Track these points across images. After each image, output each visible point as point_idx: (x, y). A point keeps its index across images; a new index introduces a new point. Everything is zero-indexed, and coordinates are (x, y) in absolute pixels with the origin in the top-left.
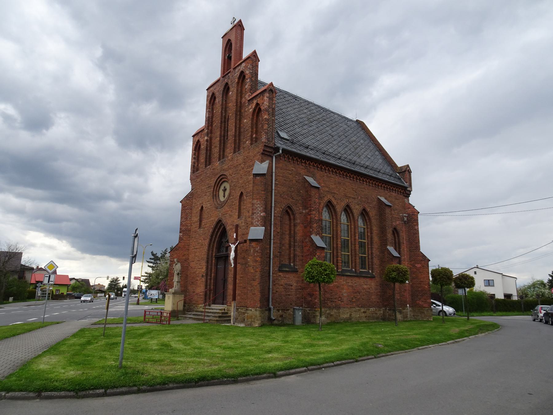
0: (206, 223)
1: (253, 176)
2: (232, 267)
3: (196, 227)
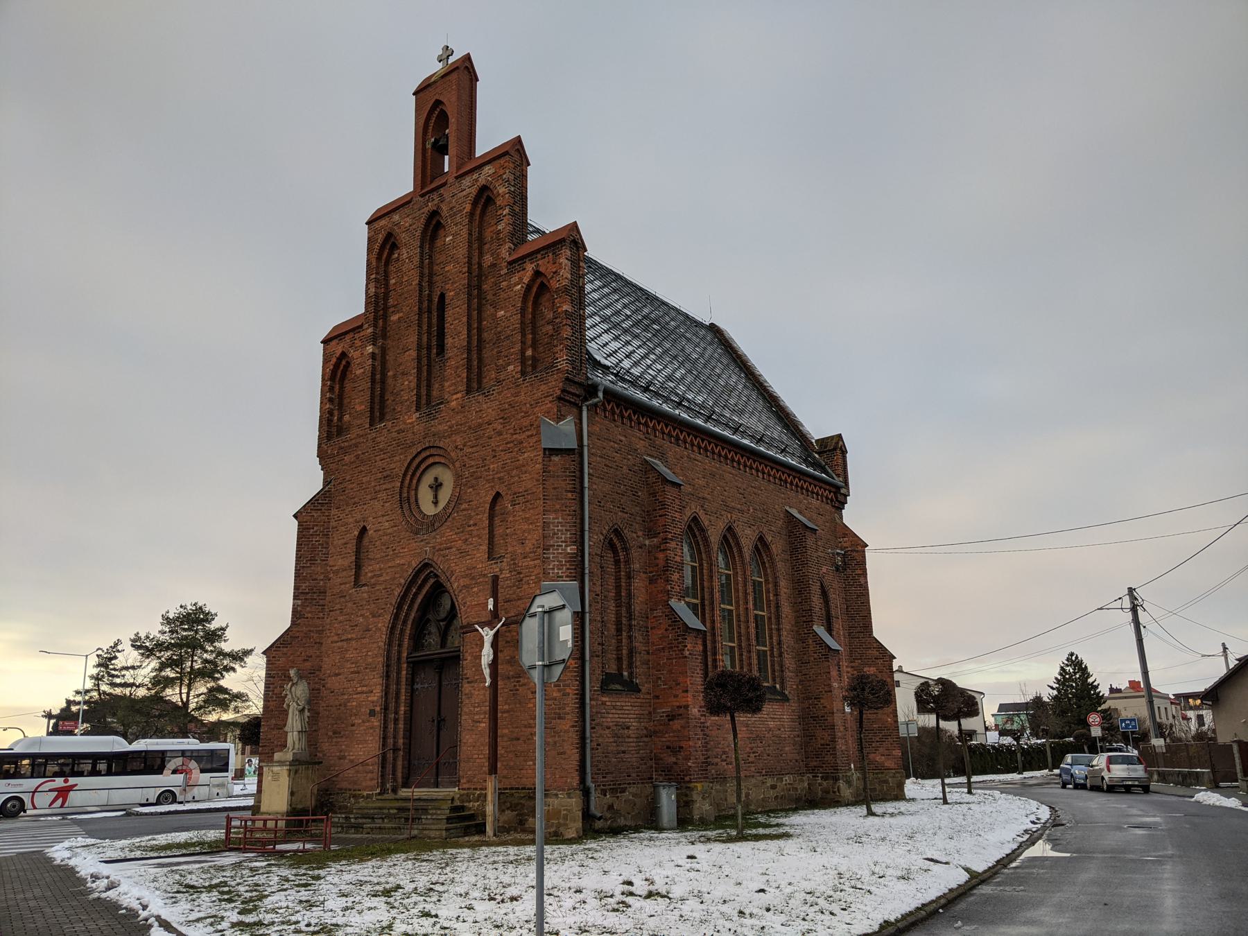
0: (379, 573)
1: (544, 454)
2: (487, 684)
3: (345, 583)
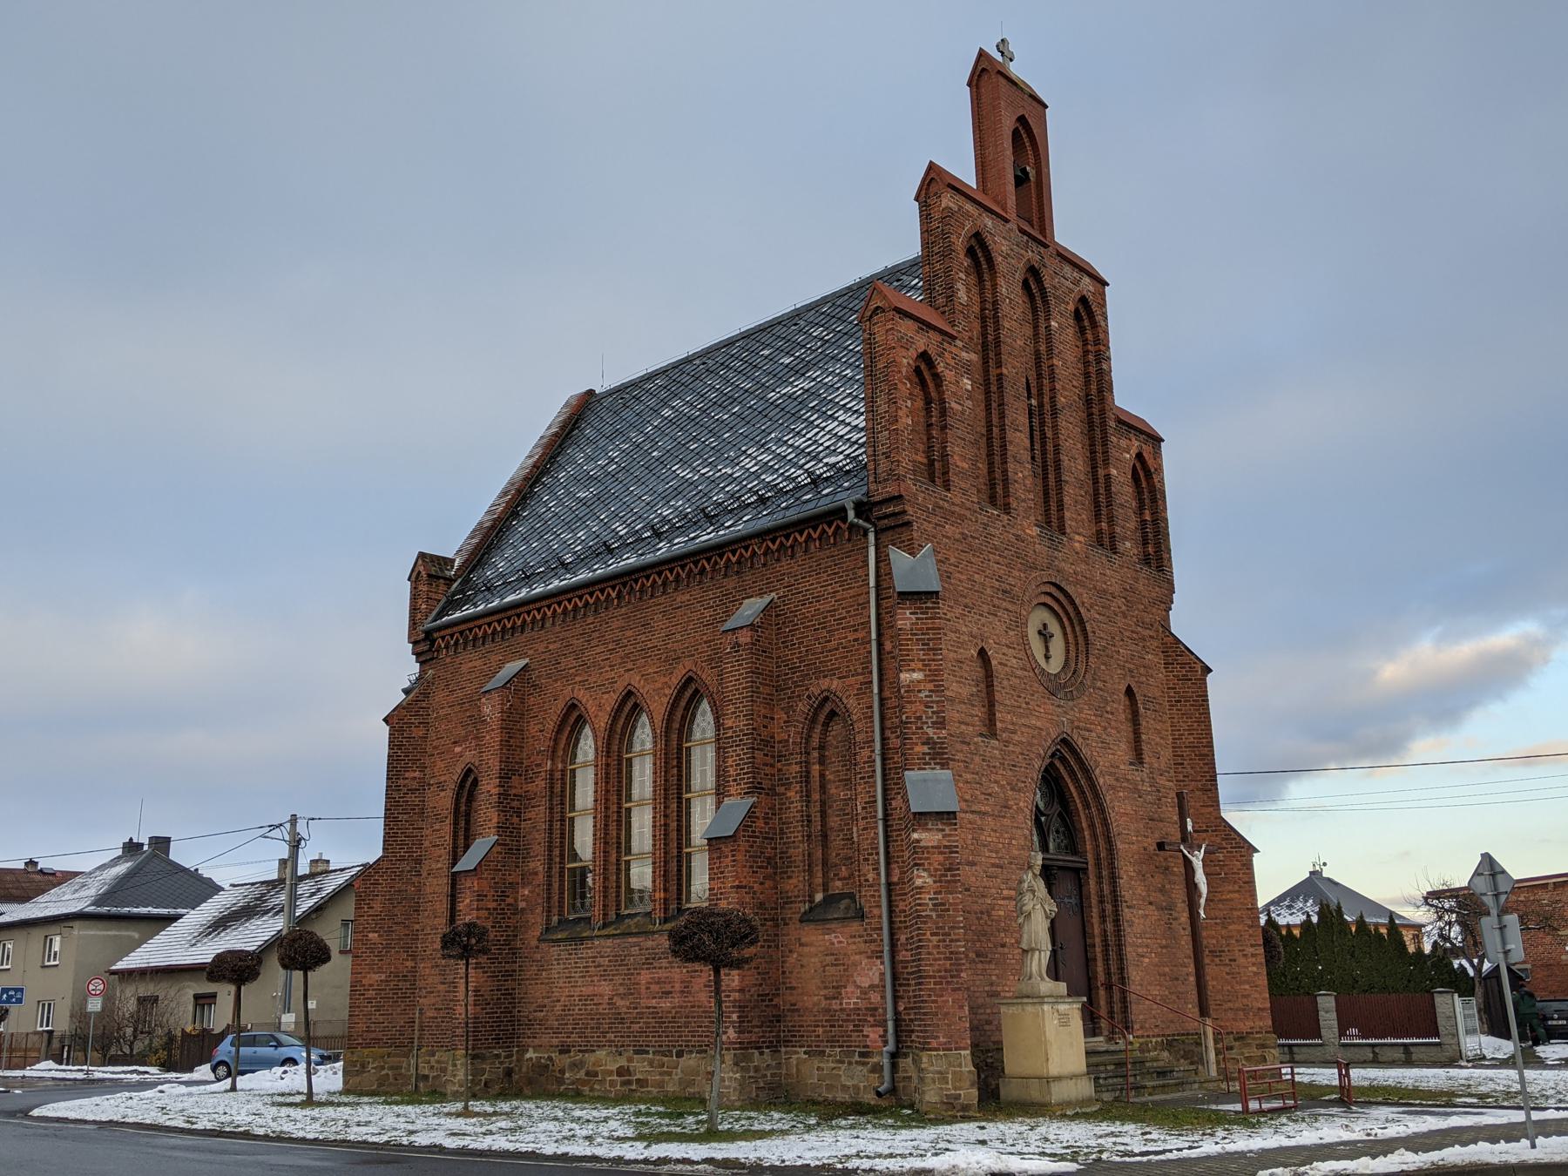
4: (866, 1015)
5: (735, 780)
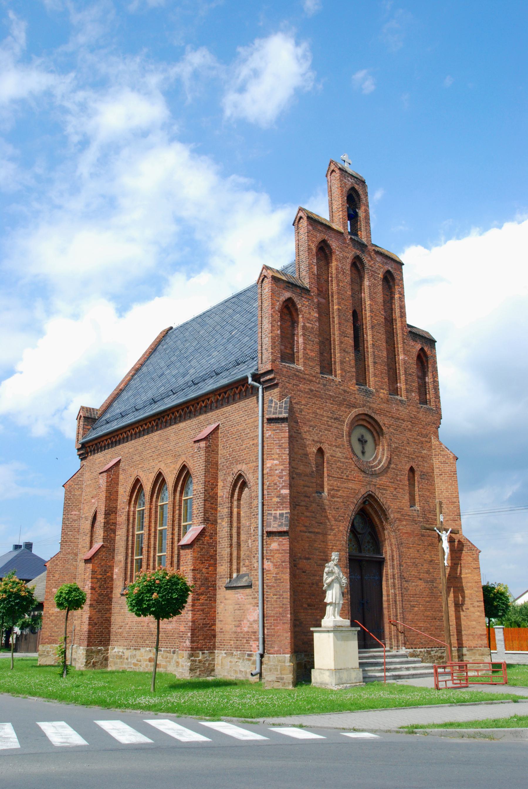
3: (309, 487)
4: (251, 635)
5: (196, 516)
